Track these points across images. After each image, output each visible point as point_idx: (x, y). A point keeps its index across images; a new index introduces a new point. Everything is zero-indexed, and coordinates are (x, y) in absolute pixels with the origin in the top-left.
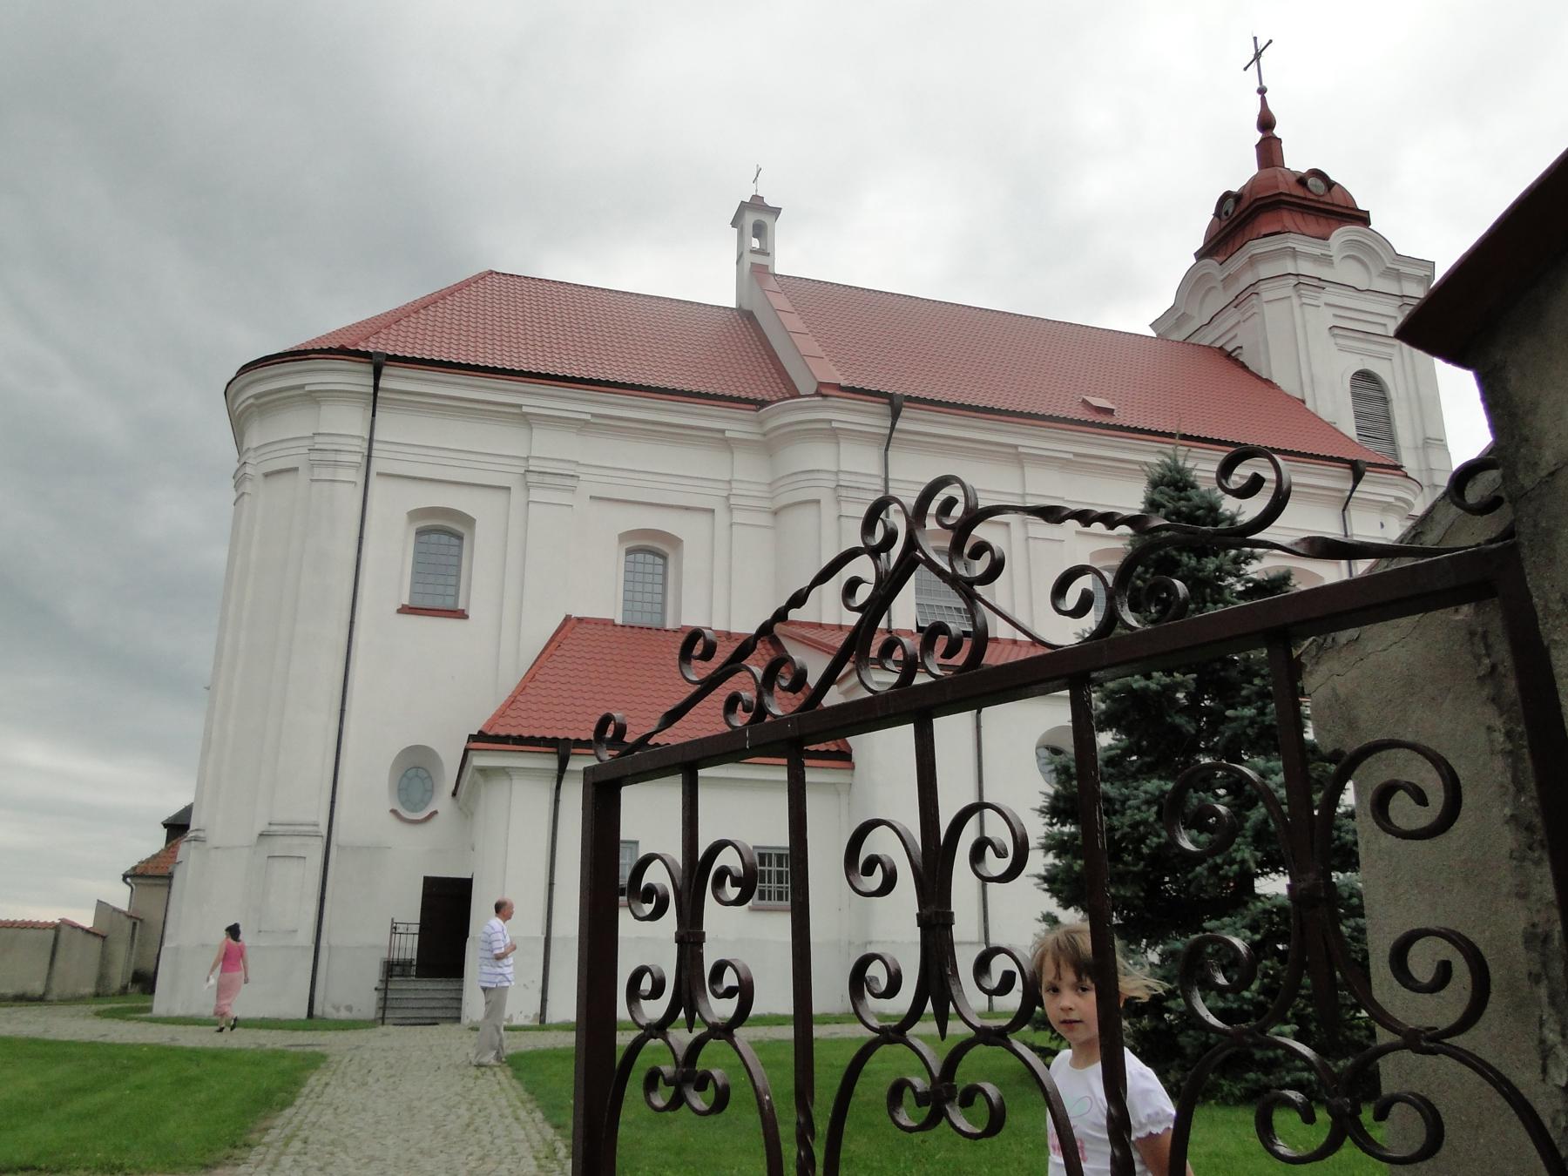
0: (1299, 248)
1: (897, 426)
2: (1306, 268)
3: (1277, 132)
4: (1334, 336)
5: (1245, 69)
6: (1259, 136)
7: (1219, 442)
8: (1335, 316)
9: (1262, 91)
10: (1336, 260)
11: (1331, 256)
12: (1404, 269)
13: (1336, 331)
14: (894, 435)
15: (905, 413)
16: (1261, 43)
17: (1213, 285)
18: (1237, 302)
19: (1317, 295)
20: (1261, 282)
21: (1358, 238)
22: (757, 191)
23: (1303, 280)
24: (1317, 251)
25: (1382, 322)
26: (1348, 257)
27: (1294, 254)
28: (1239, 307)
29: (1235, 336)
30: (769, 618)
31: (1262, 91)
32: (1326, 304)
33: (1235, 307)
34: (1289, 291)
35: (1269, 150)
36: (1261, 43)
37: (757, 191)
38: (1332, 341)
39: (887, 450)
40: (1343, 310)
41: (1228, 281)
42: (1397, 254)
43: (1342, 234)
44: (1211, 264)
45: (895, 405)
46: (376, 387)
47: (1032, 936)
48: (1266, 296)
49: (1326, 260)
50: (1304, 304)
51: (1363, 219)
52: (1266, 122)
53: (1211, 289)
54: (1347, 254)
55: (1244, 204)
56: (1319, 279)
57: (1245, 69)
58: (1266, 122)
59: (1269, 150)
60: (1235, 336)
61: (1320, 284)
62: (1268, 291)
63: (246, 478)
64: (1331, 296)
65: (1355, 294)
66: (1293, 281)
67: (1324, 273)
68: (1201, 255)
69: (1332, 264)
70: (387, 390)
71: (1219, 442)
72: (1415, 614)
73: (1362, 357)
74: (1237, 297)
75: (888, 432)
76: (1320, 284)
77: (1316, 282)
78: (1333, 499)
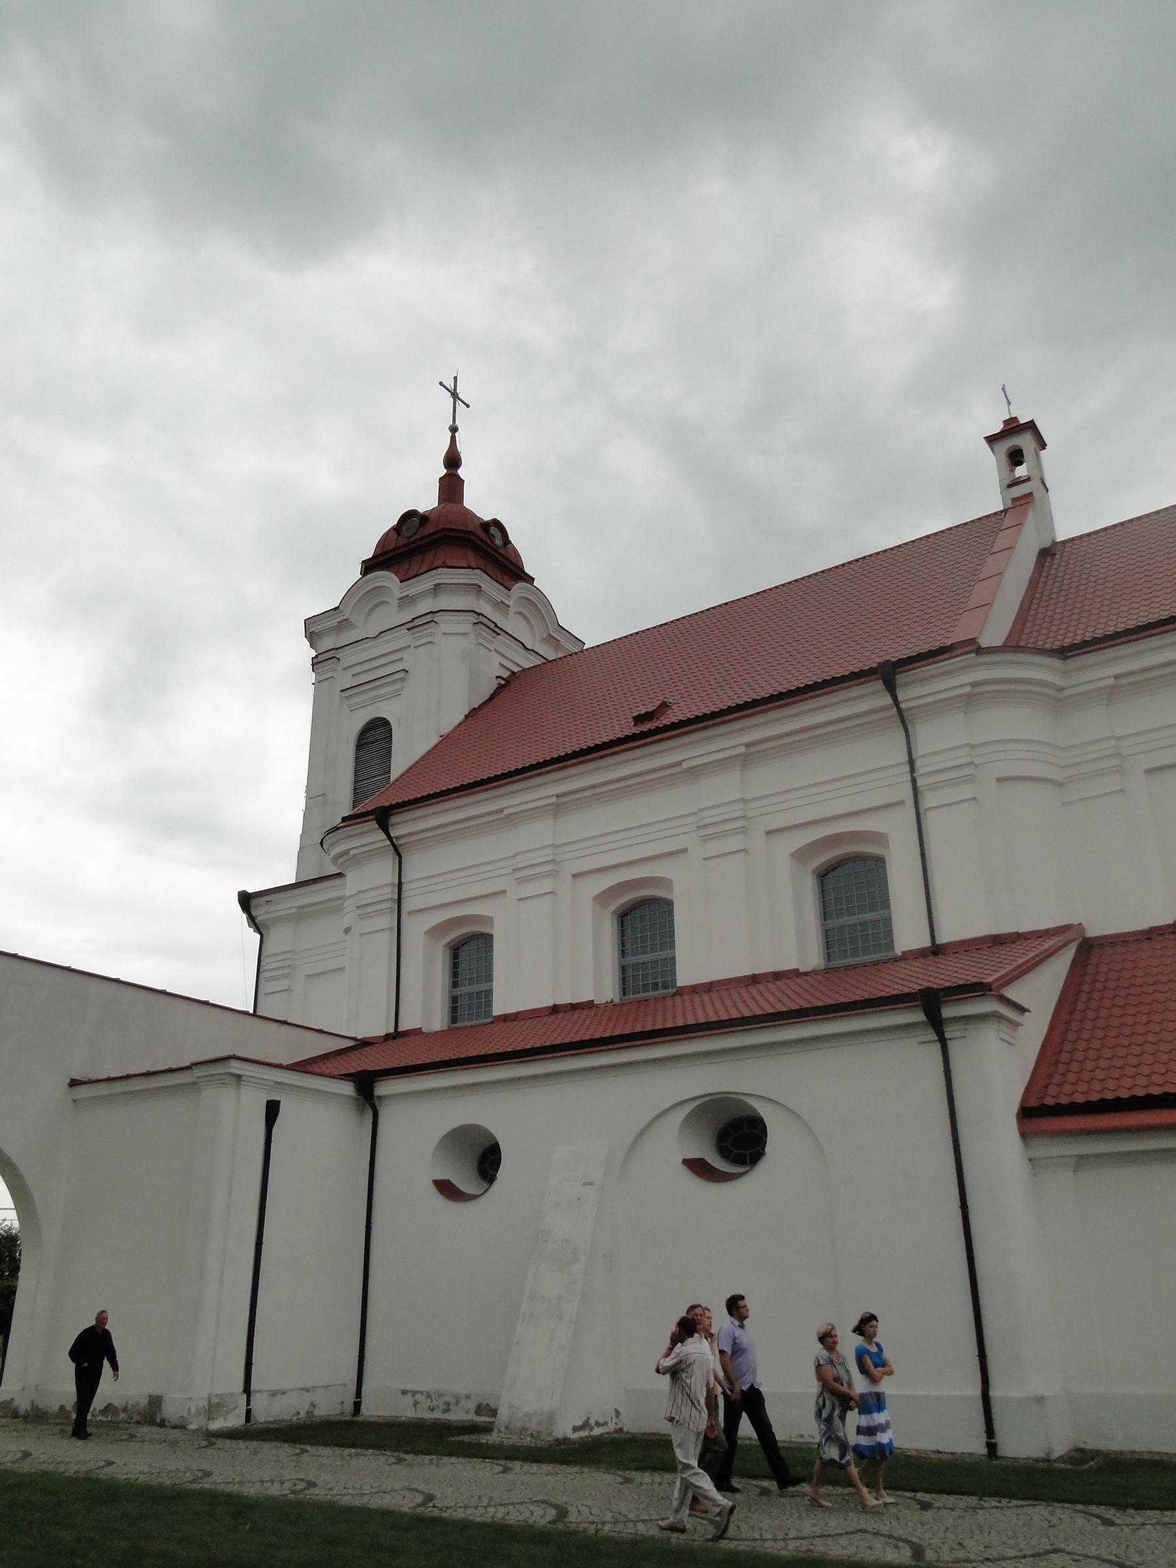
0: (484, 587)
2: (485, 608)
3: (462, 472)
5: (455, 378)
6: (443, 471)
9: (454, 430)
10: (512, 611)
11: (509, 606)
16: (450, 384)
17: (385, 584)
18: (412, 626)
19: (493, 640)
20: (441, 613)
22: (1010, 413)
23: (482, 619)
24: (499, 598)
25: (329, 676)
26: (372, 609)
28: (412, 631)
29: (401, 659)
31: (454, 430)
32: (496, 651)
33: (408, 629)
34: (467, 628)
35: (451, 486)
36: (450, 384)
37: (1010, 413)
40: (384, 658)
41: (405, 601)
44: (387, 579)
47: (854, 1334)
49: (503, 607)
51: (530, 580)
52: (453, 460)
53: (381, 603)
54: (520, 610)
55: (427, 530)
56: (496, 625)
57: (455, 378)
58: (453, 460)
59: (451, 486)
60: (401, 659)
62: (447, 624)
65: (520, 649)
66: (472, 618)
68: (369, 567)
69: (508, 614)
74: (413, 619)
76: (496, 630)
77: (492, 626)
78: (383, 850)
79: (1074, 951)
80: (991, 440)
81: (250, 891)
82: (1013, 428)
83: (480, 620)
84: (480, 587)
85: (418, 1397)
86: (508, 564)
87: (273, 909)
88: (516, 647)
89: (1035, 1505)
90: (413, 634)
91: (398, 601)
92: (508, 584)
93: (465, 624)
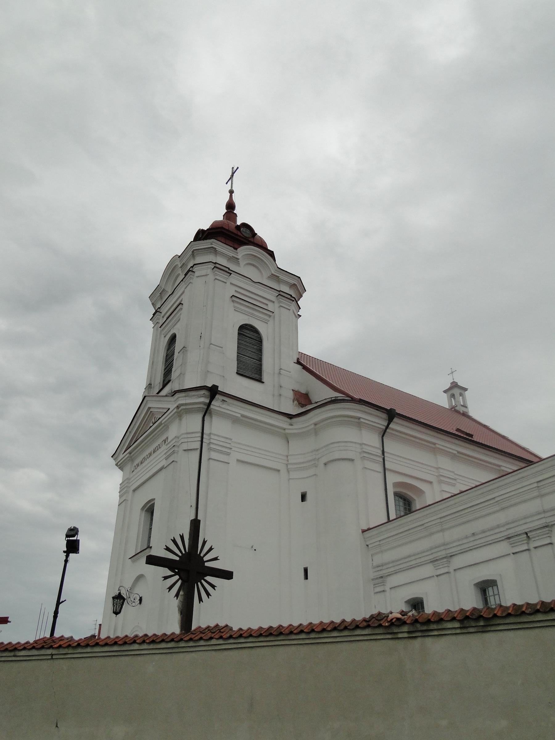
0: (218, 248)
1: (390, 426)
4: (233, 301)
7: (163, 459)
8: (236, 291)
9: (231, 192)
12: (282, 277)
13: (234, 298)
14: (388, 430)
15: (395, 420)
17: (175, 264)
19: (289, 304)
21: (255, 254)
24: (231, 254)
27: (214, 251)
30: (167, 568)
31: (231, 192)
32: (231, 283)
34: (209, 271)
35: (230, 206)
38: (232, 304)
39: (383, 436)
42: (278, 268)
43: (244, 251)
45: (391, 415)
46: (387, 427)
48: (197, 274)
49: (235, 260)
50: (282, 306)
53: (254, 265)
59: (230, 206)
61: (229, 272)
63: (174, 452)
64: (234, 279)
67: (233, 267)
69: (239, 264)
70: (393, 429)
71: (163, 459)
72: (172, 572)
73: (249, 317)
75: (384, 428)
76: (229, 272)
79: (106, 573)
80: (445, 392)
81: (459, 384)
82: (454, 385)
83: (216, 266)
84: (215, 249)
85: (131, 605)
86: (229, 233)
87: (224, 406)
88: (247, 282)
89: (434, 558)
90: (184, 282)
91: (181, 269)
92: (236, 246)
93: (207, 270)
